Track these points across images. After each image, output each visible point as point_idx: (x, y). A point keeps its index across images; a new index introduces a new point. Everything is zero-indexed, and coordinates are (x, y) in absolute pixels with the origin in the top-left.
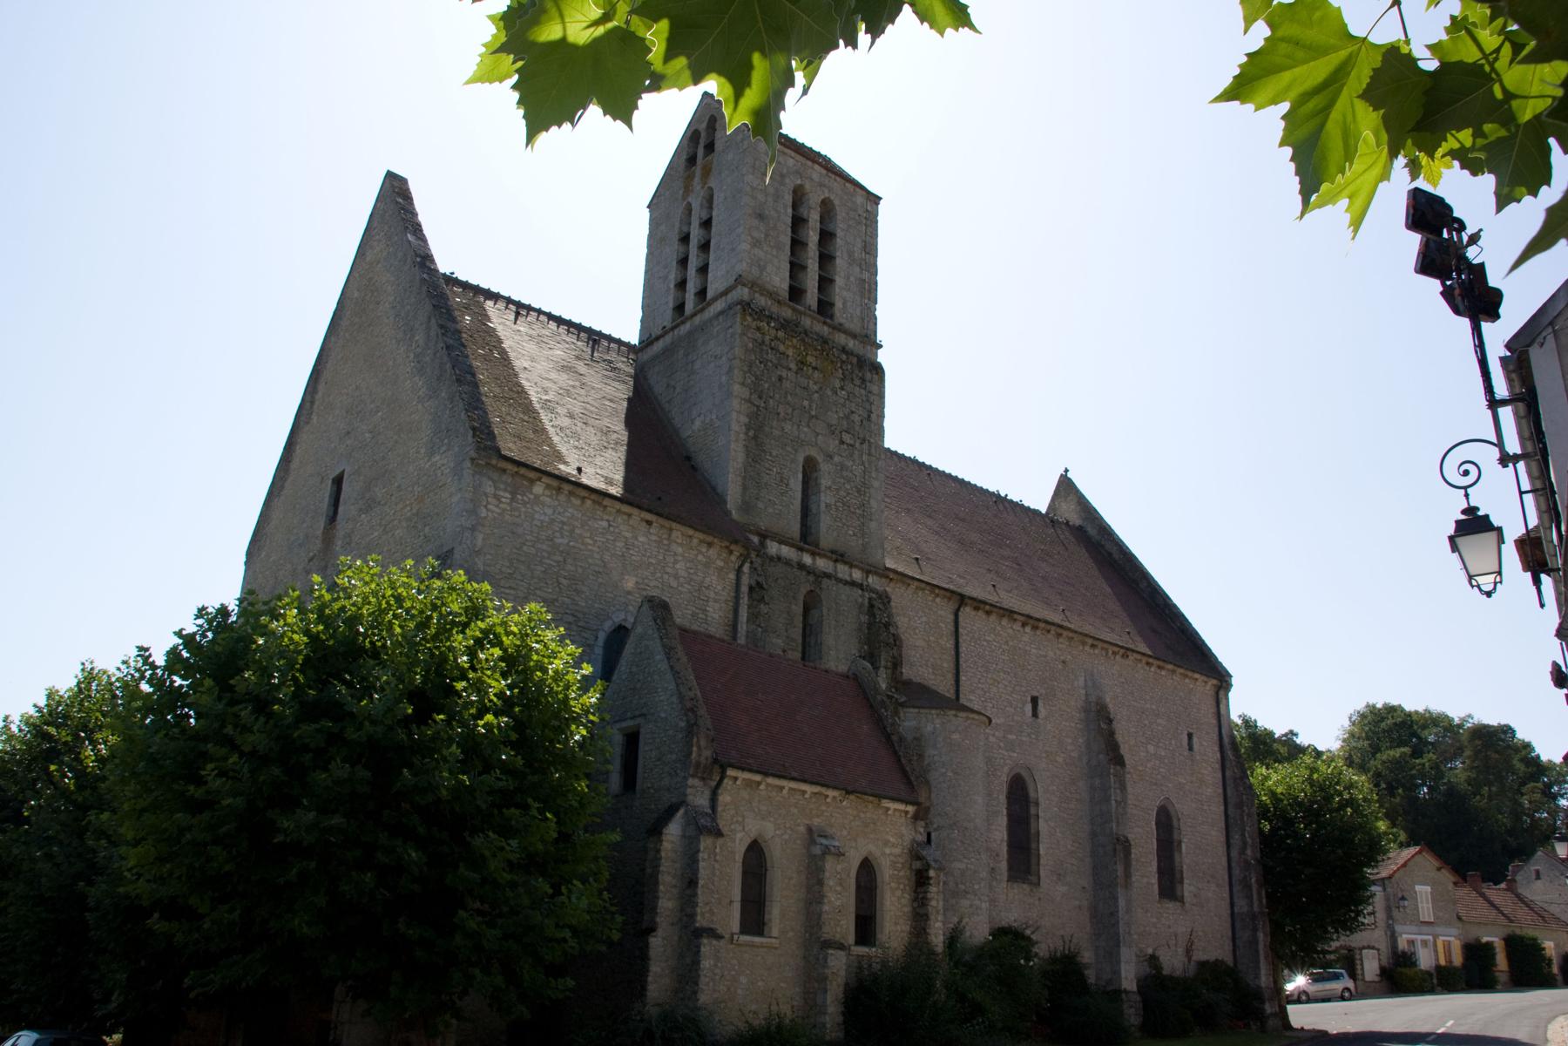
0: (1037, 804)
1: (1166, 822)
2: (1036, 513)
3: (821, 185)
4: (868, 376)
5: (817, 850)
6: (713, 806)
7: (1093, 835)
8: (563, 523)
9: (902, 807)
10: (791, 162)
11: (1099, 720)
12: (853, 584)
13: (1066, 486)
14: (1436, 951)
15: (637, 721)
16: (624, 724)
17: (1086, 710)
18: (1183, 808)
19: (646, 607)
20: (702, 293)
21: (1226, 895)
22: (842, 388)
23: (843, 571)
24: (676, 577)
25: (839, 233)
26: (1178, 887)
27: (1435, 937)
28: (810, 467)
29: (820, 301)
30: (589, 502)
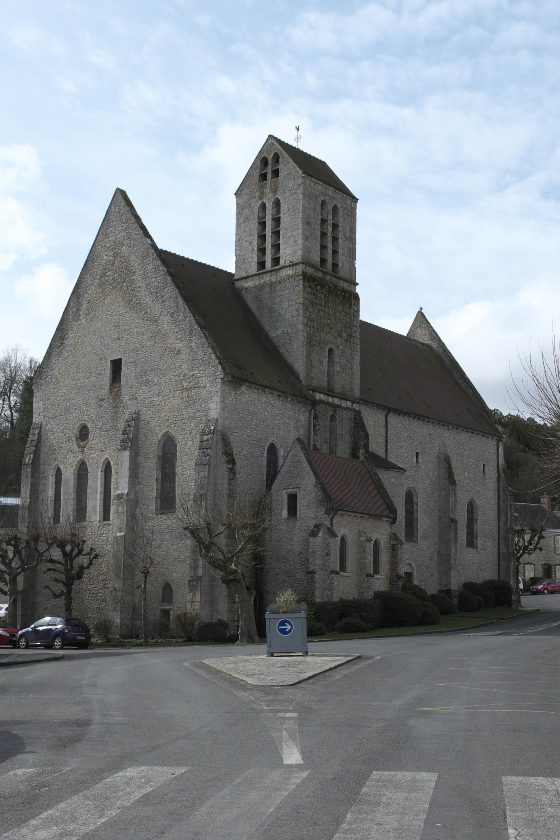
0: (417, 504)
1: (471, 508)
2: (404, 336)
3: (333, 198)
4: (353, 301)
5: (363, 539)
7: (440, 517)
8: (251, 401)
9: (388, 519)
10: (320, 188)
11: (446, 462)
12: (347, 409)
13: (421, 319)
15: (296, 490)
16: (288, 491)
17: (438, 458)
18: (479, 502)
19: (296, 442)
20: (276, 261)
21: (496, 544)
22: (343, 311)
23: (344, 404)
24: (289, 418)
25: (340, 224)
26: (475, 540)
28: (331, 351)
29: (332, 263)
30: (260, 390)
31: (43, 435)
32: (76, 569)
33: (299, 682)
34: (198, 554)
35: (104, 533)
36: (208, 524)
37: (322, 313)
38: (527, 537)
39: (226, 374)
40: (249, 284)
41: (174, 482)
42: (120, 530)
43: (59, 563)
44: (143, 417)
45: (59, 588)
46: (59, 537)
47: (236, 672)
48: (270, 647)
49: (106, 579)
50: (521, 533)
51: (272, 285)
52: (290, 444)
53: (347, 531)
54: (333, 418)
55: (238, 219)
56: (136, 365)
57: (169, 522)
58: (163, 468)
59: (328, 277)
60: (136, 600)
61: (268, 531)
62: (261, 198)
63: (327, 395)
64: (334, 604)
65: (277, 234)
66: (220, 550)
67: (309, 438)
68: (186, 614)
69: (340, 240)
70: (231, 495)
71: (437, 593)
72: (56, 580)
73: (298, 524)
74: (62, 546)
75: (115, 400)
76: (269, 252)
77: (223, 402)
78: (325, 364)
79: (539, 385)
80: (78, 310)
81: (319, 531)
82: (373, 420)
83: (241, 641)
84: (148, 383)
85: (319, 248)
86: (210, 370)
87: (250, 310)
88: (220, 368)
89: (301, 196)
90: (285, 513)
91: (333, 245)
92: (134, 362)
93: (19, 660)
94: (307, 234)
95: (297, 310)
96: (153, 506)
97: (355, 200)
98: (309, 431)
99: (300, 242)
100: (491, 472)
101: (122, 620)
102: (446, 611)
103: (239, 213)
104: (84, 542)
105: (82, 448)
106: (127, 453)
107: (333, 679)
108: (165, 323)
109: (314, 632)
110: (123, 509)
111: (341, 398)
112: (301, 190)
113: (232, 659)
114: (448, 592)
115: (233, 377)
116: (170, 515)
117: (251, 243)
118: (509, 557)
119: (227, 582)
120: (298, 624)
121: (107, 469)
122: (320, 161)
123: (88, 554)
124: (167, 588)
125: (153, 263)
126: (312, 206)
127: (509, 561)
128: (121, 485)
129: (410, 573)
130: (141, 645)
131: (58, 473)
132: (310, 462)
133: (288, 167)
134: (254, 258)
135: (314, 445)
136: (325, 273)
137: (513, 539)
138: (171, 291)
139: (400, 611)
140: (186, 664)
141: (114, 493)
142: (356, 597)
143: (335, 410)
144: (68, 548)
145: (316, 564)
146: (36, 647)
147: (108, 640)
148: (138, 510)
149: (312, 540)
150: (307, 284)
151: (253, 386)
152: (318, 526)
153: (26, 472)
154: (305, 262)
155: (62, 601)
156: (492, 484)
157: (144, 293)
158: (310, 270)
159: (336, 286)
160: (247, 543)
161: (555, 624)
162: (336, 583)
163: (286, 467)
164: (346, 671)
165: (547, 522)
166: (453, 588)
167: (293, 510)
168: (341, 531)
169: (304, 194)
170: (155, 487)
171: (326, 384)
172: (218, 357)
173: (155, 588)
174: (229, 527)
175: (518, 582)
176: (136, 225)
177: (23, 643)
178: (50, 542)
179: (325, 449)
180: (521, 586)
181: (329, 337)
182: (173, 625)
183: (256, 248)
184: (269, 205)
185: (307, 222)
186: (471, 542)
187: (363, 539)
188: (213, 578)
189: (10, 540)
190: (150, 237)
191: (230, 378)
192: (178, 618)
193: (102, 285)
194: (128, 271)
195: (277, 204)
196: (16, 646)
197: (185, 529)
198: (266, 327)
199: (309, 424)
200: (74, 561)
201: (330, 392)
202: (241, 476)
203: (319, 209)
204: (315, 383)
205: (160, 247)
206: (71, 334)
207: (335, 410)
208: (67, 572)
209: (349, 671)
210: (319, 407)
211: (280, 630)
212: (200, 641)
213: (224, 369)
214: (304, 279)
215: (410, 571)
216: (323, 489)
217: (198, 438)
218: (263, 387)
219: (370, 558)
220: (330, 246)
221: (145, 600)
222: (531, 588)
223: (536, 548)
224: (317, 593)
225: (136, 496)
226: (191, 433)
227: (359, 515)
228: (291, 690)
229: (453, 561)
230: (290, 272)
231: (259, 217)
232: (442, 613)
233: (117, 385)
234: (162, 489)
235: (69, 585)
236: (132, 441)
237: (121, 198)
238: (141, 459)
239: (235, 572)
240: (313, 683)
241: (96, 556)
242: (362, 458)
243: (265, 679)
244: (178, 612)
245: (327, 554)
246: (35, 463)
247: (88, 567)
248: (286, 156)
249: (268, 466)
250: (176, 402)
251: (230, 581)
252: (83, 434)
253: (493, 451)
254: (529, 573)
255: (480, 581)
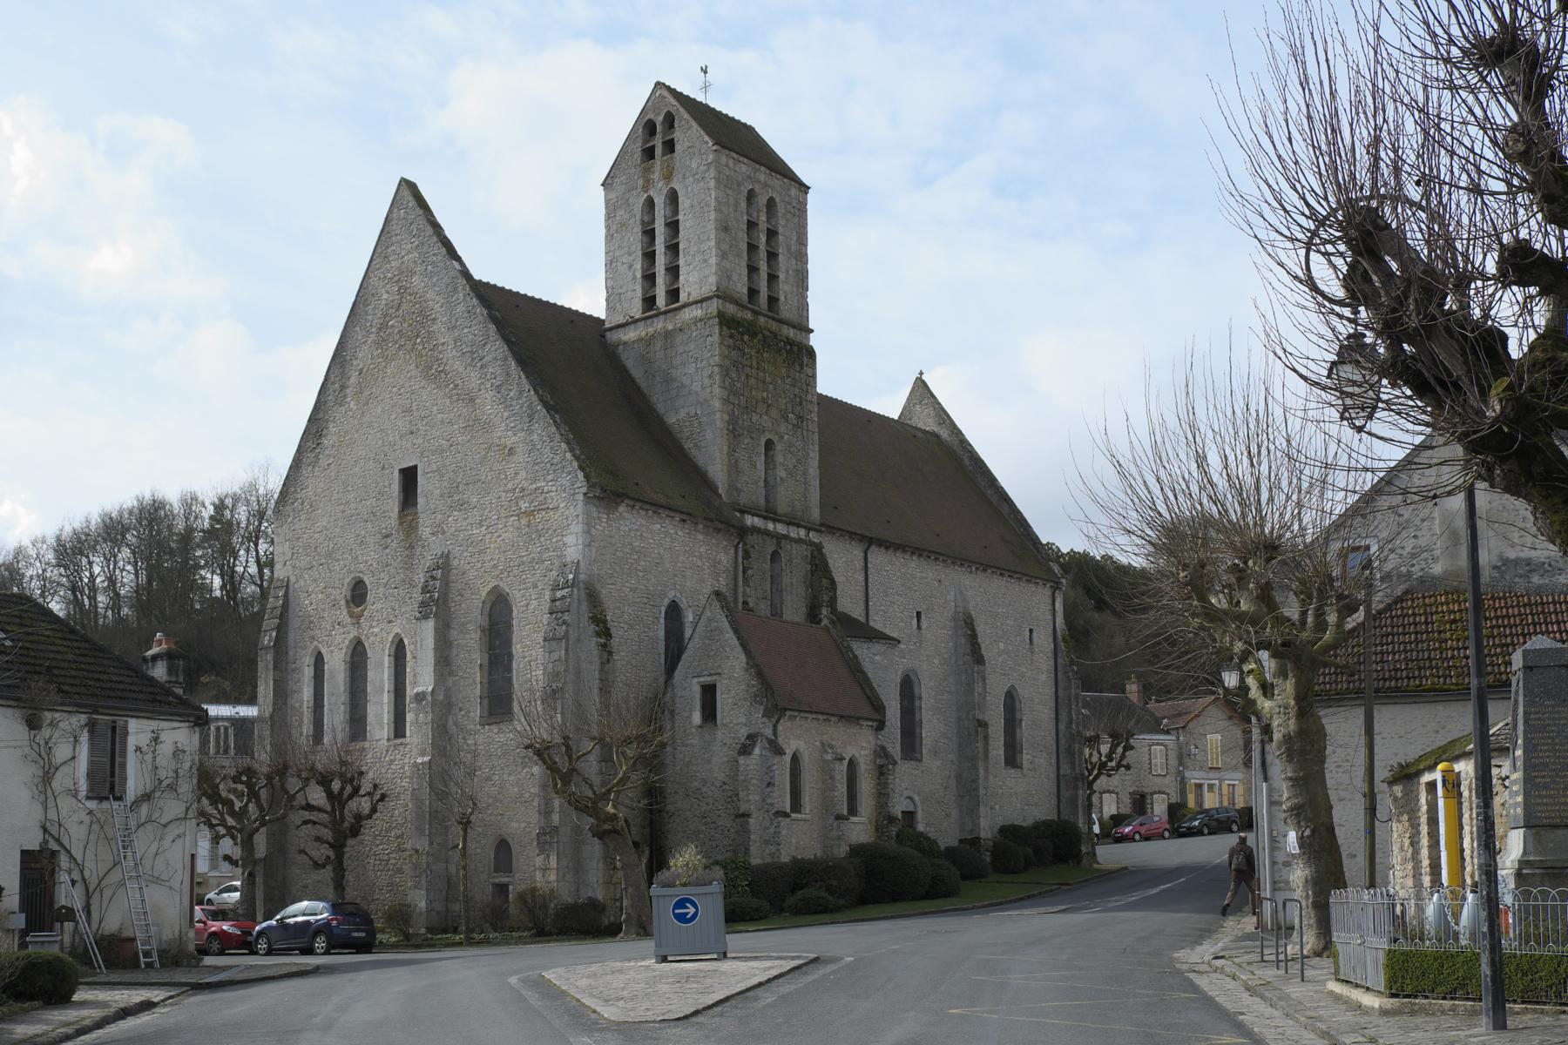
3: (766, 185)
4: (805, 360)
5: (829, 757)
6: (775, 734)
7: (959, 719)
10: (744, 168)
11: (967, 626)
12: (799, 541)
13: (921, 389)
14: (1221, 795)
17: (954, 619)
18: (1023, 692)
20: (673, 294)
21: (1054, 761)
23: (794, 532)
24: (700, 557)
25: (781, 230)
27: (1221, 780)
28: (769, 445)
31: (291, 599)
32: (349, 819)
33: (696, 1013)
34: (550, 789)
35: (395, 759)
36: (566, 738)
37: (752, 381)
38: (1105, 749)
39: (591, 486)
40: (630, 335)
41: (510, 670)
42: (423, 754)
43: (320, 810)
44: (455, 563)
45: (322, 852)
46: (319, 766)
47: (592, 995)
48: (659, 945)
49: (401, 836)
50: (1094, 741)
51: (668, 335)
52: (703, 601)
53: (802, 744)
54: (775, 556)
55: (608, 227)
56: (442, 476)
57: (502, 738)
58: (491, 647)
59: (762, 320)
60: (453, 869)
61: (669, 749)
62: (645, 189)
63: (766, 518)
64: (781, 867)
65: (673, 249)
66: (586, 780)
67: (735, 590)
68: (533, 890)
69: (781, 258)
70: (605, 690)
71: (956, 843)
72: (318, 839)
73: (719, 734)
74: (325, 782)
75: (408, 535)
76: (661, 281)
77: (588, 532)
78: (761, 465)
79: (1122, 473)
80: (343, 387)
81: (753, 746)
82: (842, 558)
83: (627, 933)
84: (461, 505)
85: (745, 271)
86: (565, 480)
87: (632, 380)
88: (581, 475)
89: (712, 184)
90: (697, 717)
91: (769, 266)
92: (438, 470)
93: (240, 977)
94: (725, 247)
95: (710, 377)
96: (477, 712)
97: (805, 188)
98: (735, 579)
99: (713, 261)
100: (1044, 641)
101: (430, 902)
102: (972, 874)
103: (609, 216)
104: (361, 774)
105: (356, 618)
106: (429, 626)
107: (760, 1004)
108: (488, 403)
109: (737, 917)
110: (426, 717)
111: (788, 524)
112: (712, 173)
113: (594, 967)
114: (975, 842)
115: (604, 490)
116: (504, 726)
117: (630, 267)
118: (1076, 781)
119: (601, 835)
120: (710, 903)
121: (399, 653)
122: (745, 125)
123: (369, 794)
124: (503, 848)
125: (464, 302)
126: (732, 201)
127: (1076, 788)
128: (422, 678)
129: (911, 813)
130: (460, 944)
131: (319, 660)
132: (736, 631)
133: (689, 134)
134: (637, 291)
135: (745, 603)
136: (756, 313)
137: (1082, 753)
138: (496, 349)
139: (894, 877)
140: (513, 980)
141: (410, 691)
142: (819, 854)
143: (779, 544)
144: (336, 785)
145: (751, 800)
146: (286, 952)
147: (407, 937)
148: (451, 720)
149: (742, 760)
150: (726, 331)
151: (638, 505)
152: (752, 738)
153: (266, 661)
154: (721, 295)
155: (327, 873)
156: (1044, 660)
157: (450, 353)
158: (731, 309)
159: (775, 335)
160: (633, 767)
161: (1154, 891)
162: (784, 832)
163: (697, 638)
164: (786, 987)
165: (1137, 722)
166: (983, 835)
167: (709, 712)
168: (791, 745)
169: (717, 180)
170: (478, 679)
171: (762, 501)
172: (577, 458)
173: (481, 849)
174: (600, 741)
175: (1090, 823)
176: (435, 239)
177: (262, 946)
178: (304, 775)
179: (763, 609)
180: (1096, 829)
181: (766, 421)
182: (513, 909)
183: (639, 275)
184: (659, 201)
185: (724, 228)
186: (1012, 760)
187: (829, 757)
188: (577, 830)
189: (240, 774)
190: (458, 259)
191: (598, 492)
192: (521, 897)
193: (380, 343)
194: (424, 316)
195: (673, 198)
196: (253, 952)
197: (527, 747)
198: (661, 408)
199: (736, 568)
200: (346, 803)
201: (770, 513)
202: (621, 658)
203: (743, 205)
204: (743, 500)
205: (476, 277)
206: (332, 428)
207: (779, 544)
208: (336, 824)
209: (793, 987)
210: (752, 539)
211: (676, 916)
212: (558, 934)
213: (587, 477)
214: (721, 324)
215: (911, 808)
216: (760, 674)
217: (547, 595)
218: (656, 507)
219: (842, 788)
220: (763, 266)
221: (464, 868)
222: (1113, 832)
223: (1119, 766)
224: (753, 849)
225: (448, 696)
226: (535, 586)
227: (821, 717)
228: (677, 1031)
229: (982, 791)
230: (697, 312)
231: (643, 222)
232: (964, 878)
233: (411, 510)
234: (490, 682)
235: (338, 846)
236: (437, 603)
237: (409, 190)
238: (454, 634)
239: (614, 817)
240: (721, 1015)
241: (383, 797)
242: (825, 622)
243: (634, 1009)
244: (520, 888)
245: (769, 784)
246: (280, 646)
247: (369, 817)
248: (686, 116)
249: (667, 639)
250: (509, 535)
251: (606, 832)
252: (358, 594)
253: (1045, 607)
254: (1110, 808)
255: (1028, 822)
